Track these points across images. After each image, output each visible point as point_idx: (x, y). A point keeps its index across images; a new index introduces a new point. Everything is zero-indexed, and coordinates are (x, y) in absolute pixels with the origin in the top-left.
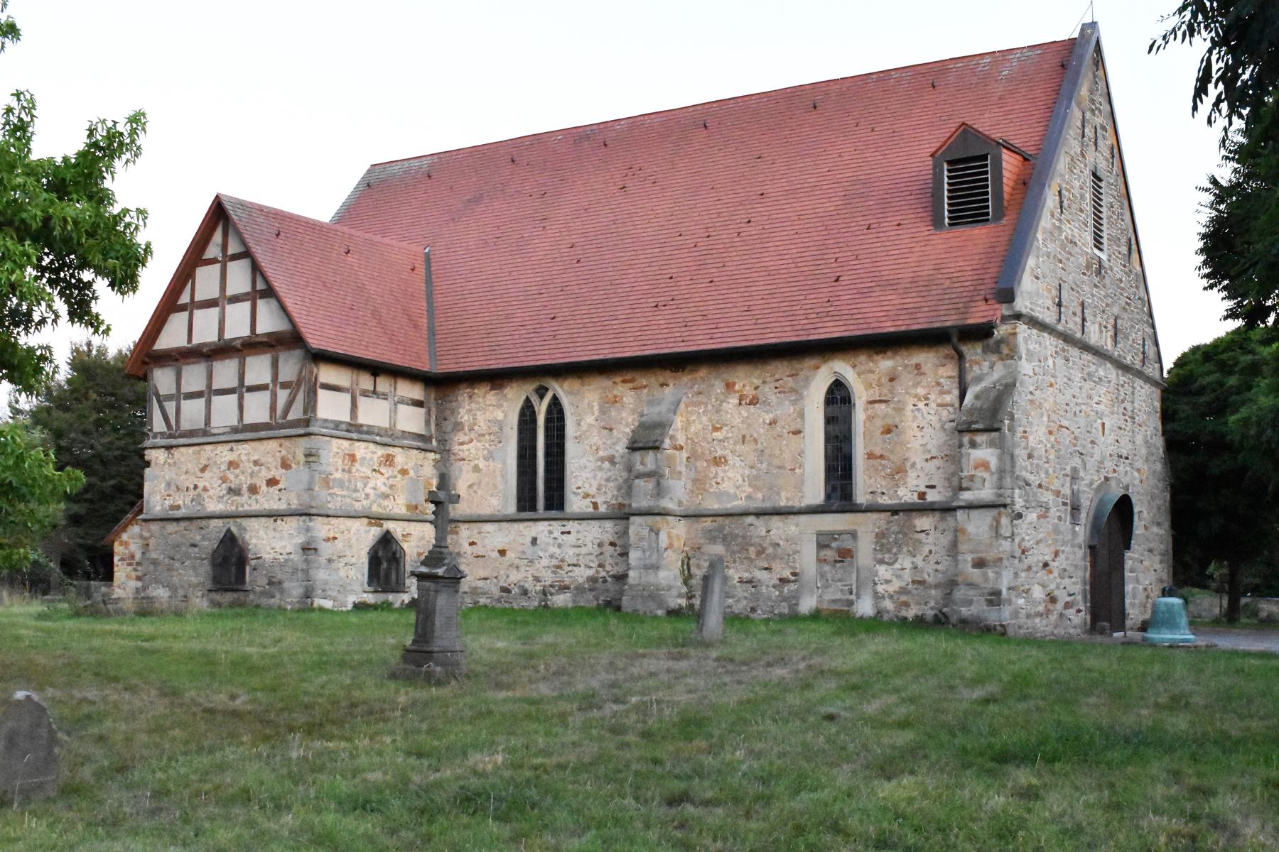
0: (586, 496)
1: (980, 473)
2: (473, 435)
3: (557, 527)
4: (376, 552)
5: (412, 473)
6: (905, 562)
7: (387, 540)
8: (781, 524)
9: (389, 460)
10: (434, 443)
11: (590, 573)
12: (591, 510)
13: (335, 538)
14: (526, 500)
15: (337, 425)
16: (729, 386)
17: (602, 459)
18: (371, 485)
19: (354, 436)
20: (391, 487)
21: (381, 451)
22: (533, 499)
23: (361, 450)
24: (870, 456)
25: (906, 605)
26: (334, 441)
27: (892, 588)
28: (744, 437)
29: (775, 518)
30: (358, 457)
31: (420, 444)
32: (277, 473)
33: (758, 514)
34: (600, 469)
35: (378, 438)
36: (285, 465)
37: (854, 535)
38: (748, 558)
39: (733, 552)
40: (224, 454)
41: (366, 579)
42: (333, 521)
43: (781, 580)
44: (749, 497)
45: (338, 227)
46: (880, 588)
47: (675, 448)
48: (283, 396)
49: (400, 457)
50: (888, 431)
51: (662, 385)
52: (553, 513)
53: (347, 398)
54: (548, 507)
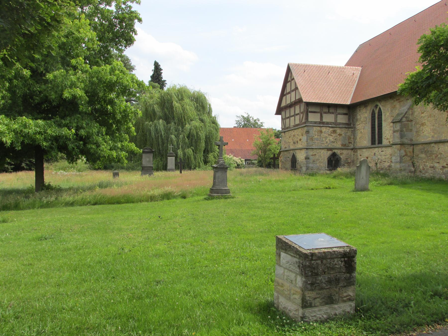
0: (387, 139)
2: (360, 122)
3: (380, 150)
4: (330, 159)
5: (343, 135)
7: (334, 155)
8: (442, 146)
9: (334, 132)
10: (352, 125)
11: (388, 164)
12: (388, 144)
13: (315, 155)
14: (373, 142)
15: (315, 123)
18: (328, 139)
19: (321, 125)
20: (335, 139)
21: (331, 129)
22: (375, 141)
23: (324, 129)
26: (314, 128)
28: (431, 115)
29: (441, 144)
30: (323, 131)
31: (346, 126)
32: (301, 137)
33: (436, 143)
35: (330, 126)
38: (432, 159)
39: (428, 157)
41: (327, 166)
42: (314, 150)
43: (443, 167)
44: (433, 137)
45: (347, 67)
47: (408, 121)
48: (301, 115)
49: (338, 131)
51: (407, 100)
52: (380, 145)
53: (319, 114)
54: (379, 143)
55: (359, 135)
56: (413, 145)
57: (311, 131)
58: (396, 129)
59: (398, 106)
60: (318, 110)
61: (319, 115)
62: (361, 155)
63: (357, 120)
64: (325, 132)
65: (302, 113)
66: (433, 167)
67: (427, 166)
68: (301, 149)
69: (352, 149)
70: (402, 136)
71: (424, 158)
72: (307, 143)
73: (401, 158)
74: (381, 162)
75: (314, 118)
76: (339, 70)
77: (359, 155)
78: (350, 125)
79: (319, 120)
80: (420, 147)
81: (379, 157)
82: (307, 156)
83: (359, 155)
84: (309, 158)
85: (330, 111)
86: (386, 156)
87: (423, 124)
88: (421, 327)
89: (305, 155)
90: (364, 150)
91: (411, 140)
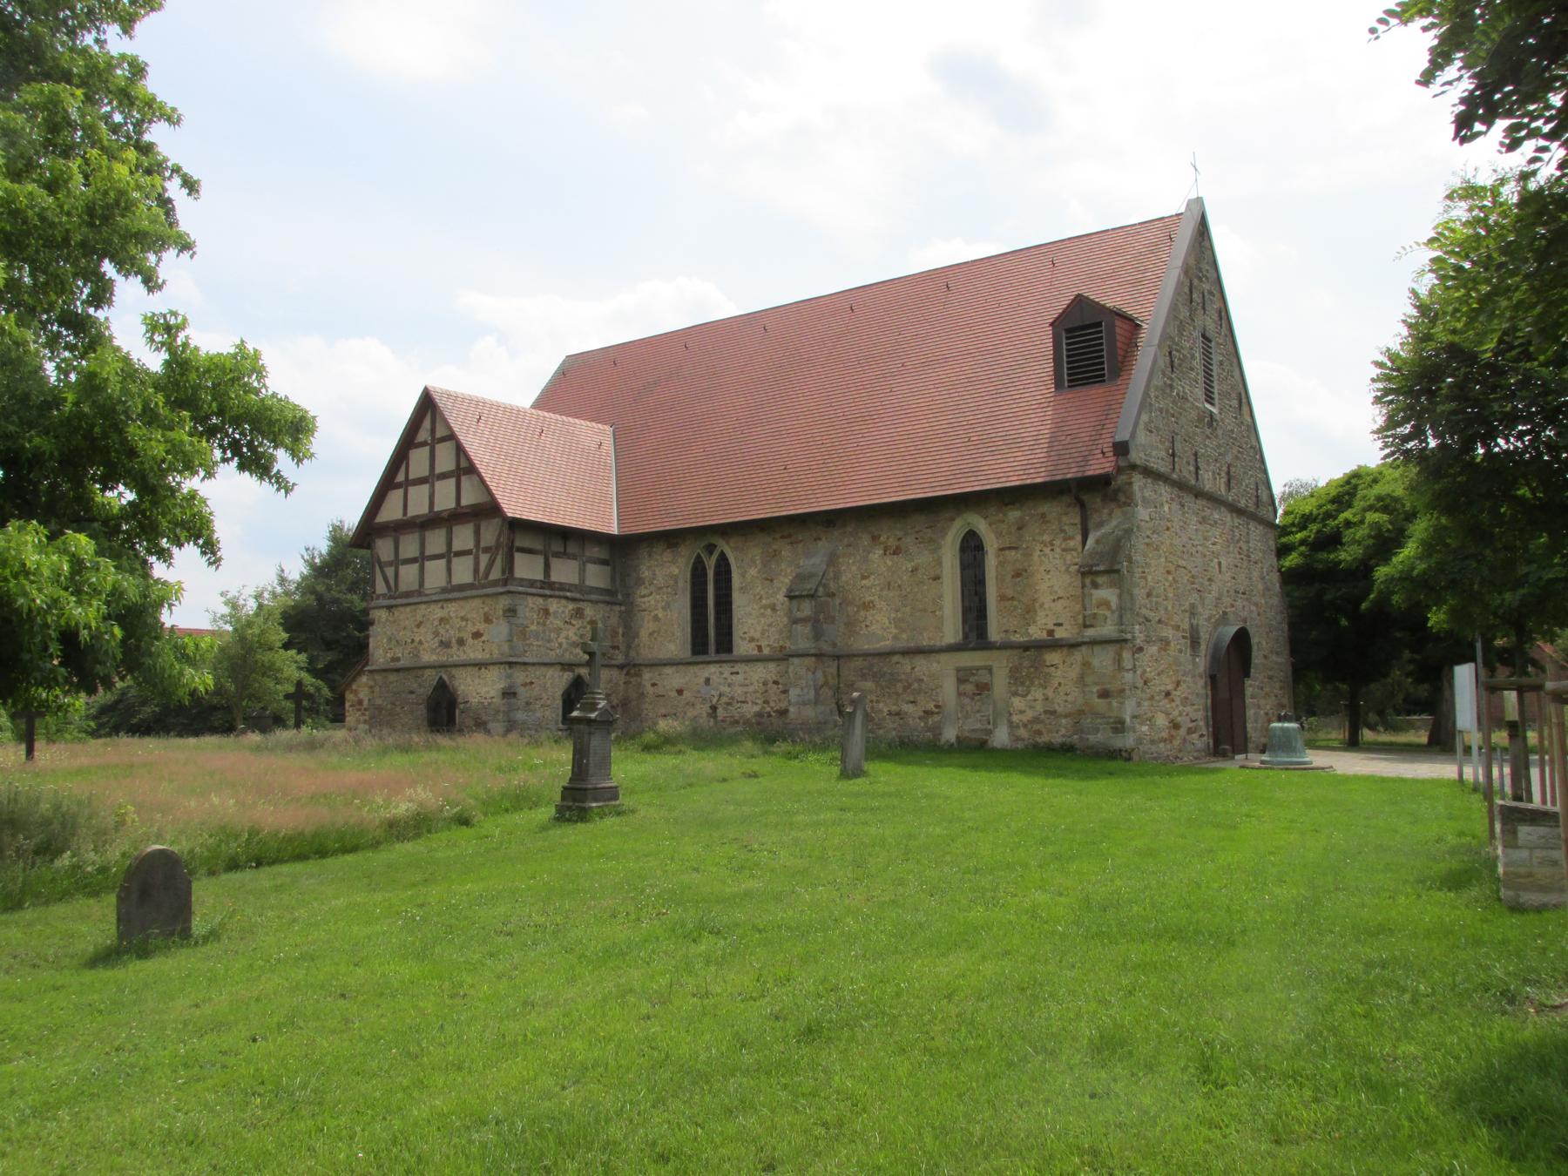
1: (1102, 611)
2: (652, 588)
3: (727, 669)
6: (1037, 693)
9: (579, 613)
14: (699, 644)
15: (532, 583)
16: (875, 538)
17: (765, 607)
19: (547, 592)
21: (571, 606)
23: (553, 605)
24: (1003, 598)
25: (1039, 733)
26: (530, 600)
27: (1025, 718)
32: (481, 627)
34: (763, 615)
36: (488, 620)
37: (990, 670)
38: (897, 694)
40: (437, 612)
43: (926, 712)
44: (895, 638)
46: (1015, 718)
49: (589, 611)
50: (1018, 575)
52: (724, 656)
55: (646, 627)
56: (838, 657)
57: (521, 611)
58: (799, 615)
59: (786, 552)
60: (537, 544)
61: (540, 560)
62: (654, 685)
63: (640, 582)
64: (555, 613)
65: (486, 550)
66: (898, 714)
67: (881, 711)
68: (480, 665)
69: (621, 667)
70: (818, 635)
71: (871, 692)
72: (511, 647)
73: (817, 689)
74: (729, 704)
75: (527, 568)
76: (512, 413)
77: (648, 685)
78: (619, 595)
79: (540, 577)
80: (859, 663)
81: (726, 689)
82: (510, 687)
83: (648, 685)
84: (515, 694)
85: (570, 550)
86: (740, 685)
87: (867, 606)
88: (1455, 864)
89: (501, 685)
90: (668, 670)
91: (834, 645)
